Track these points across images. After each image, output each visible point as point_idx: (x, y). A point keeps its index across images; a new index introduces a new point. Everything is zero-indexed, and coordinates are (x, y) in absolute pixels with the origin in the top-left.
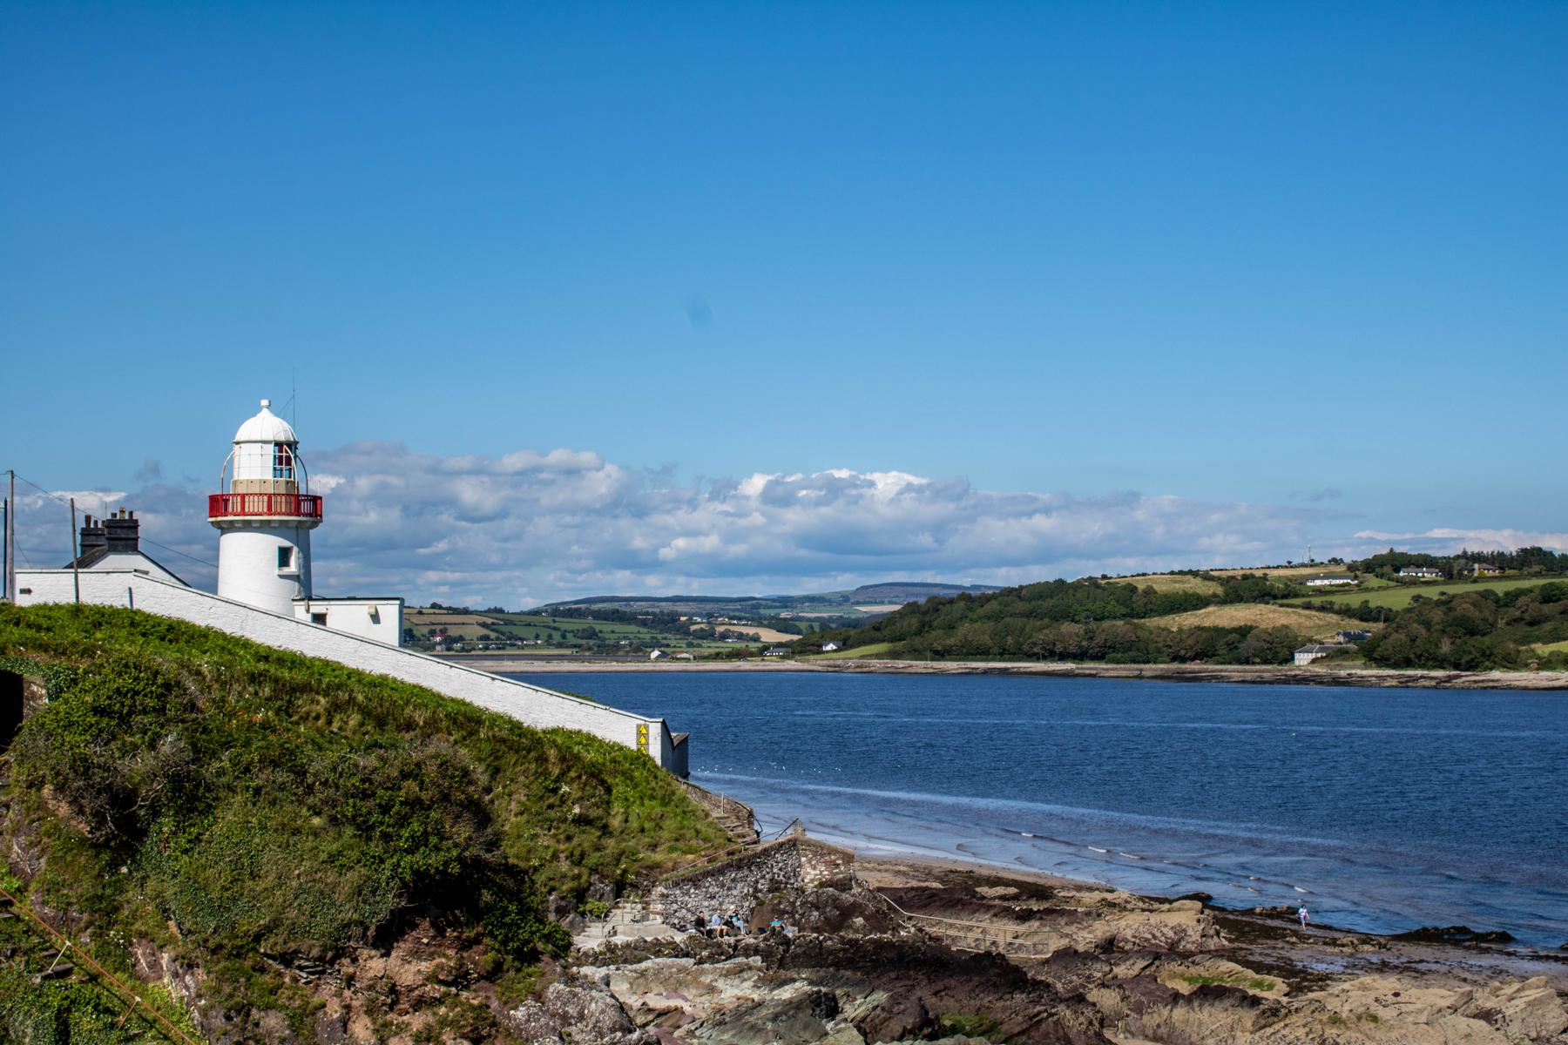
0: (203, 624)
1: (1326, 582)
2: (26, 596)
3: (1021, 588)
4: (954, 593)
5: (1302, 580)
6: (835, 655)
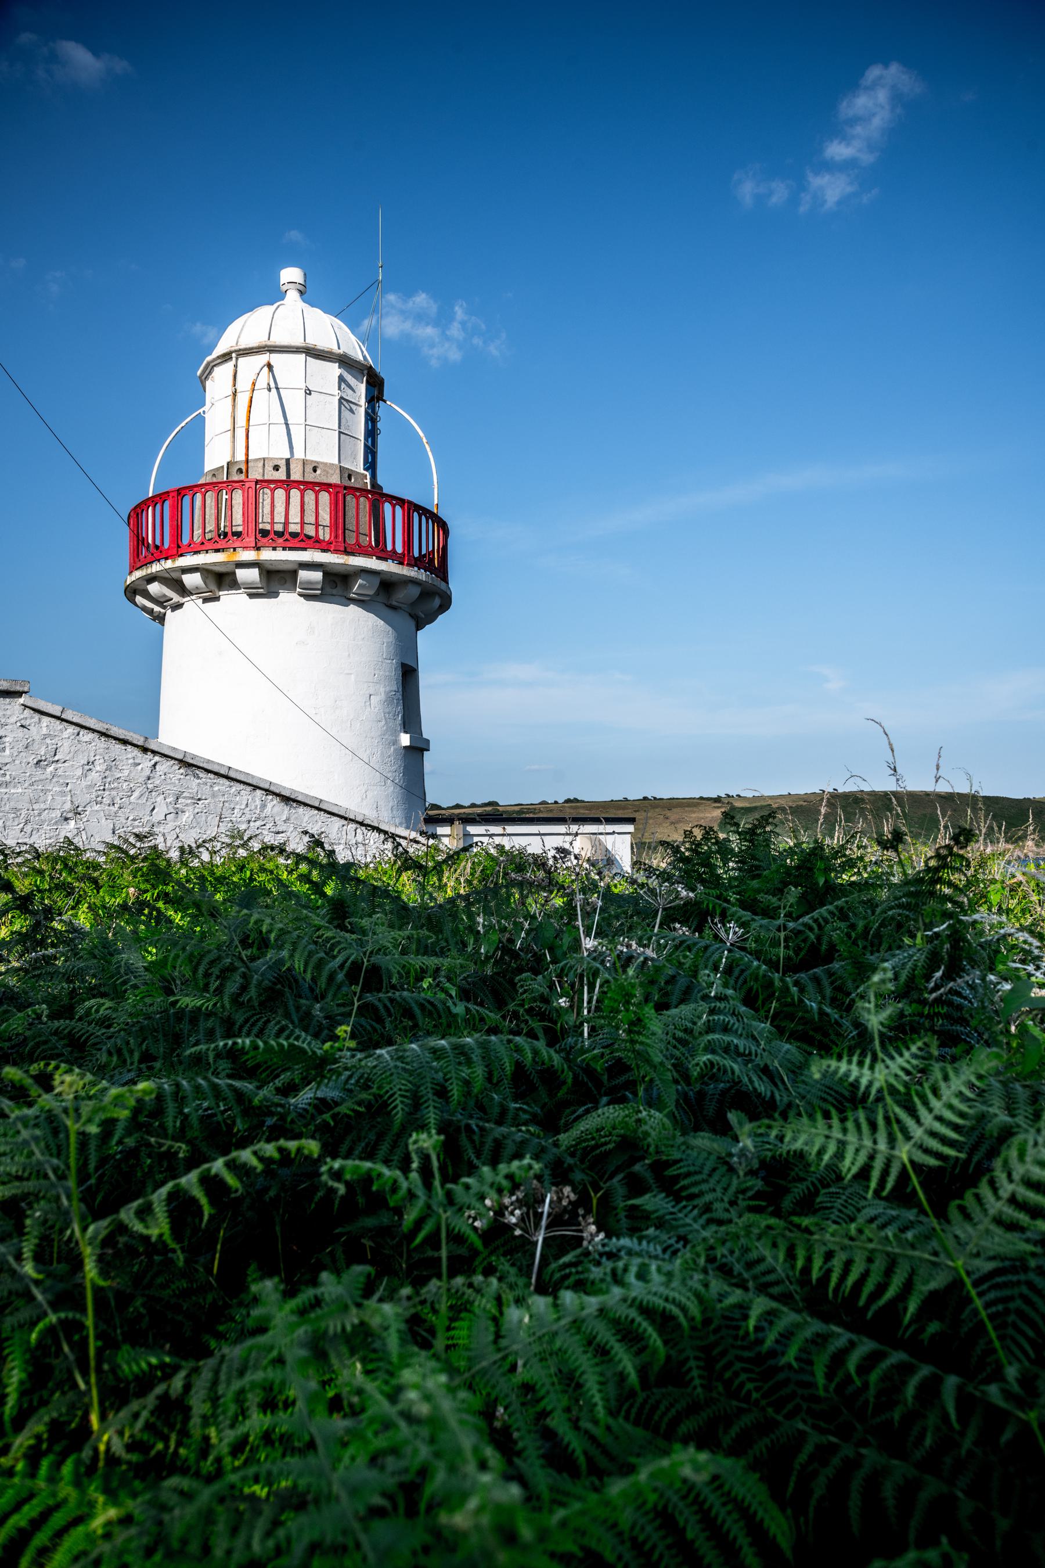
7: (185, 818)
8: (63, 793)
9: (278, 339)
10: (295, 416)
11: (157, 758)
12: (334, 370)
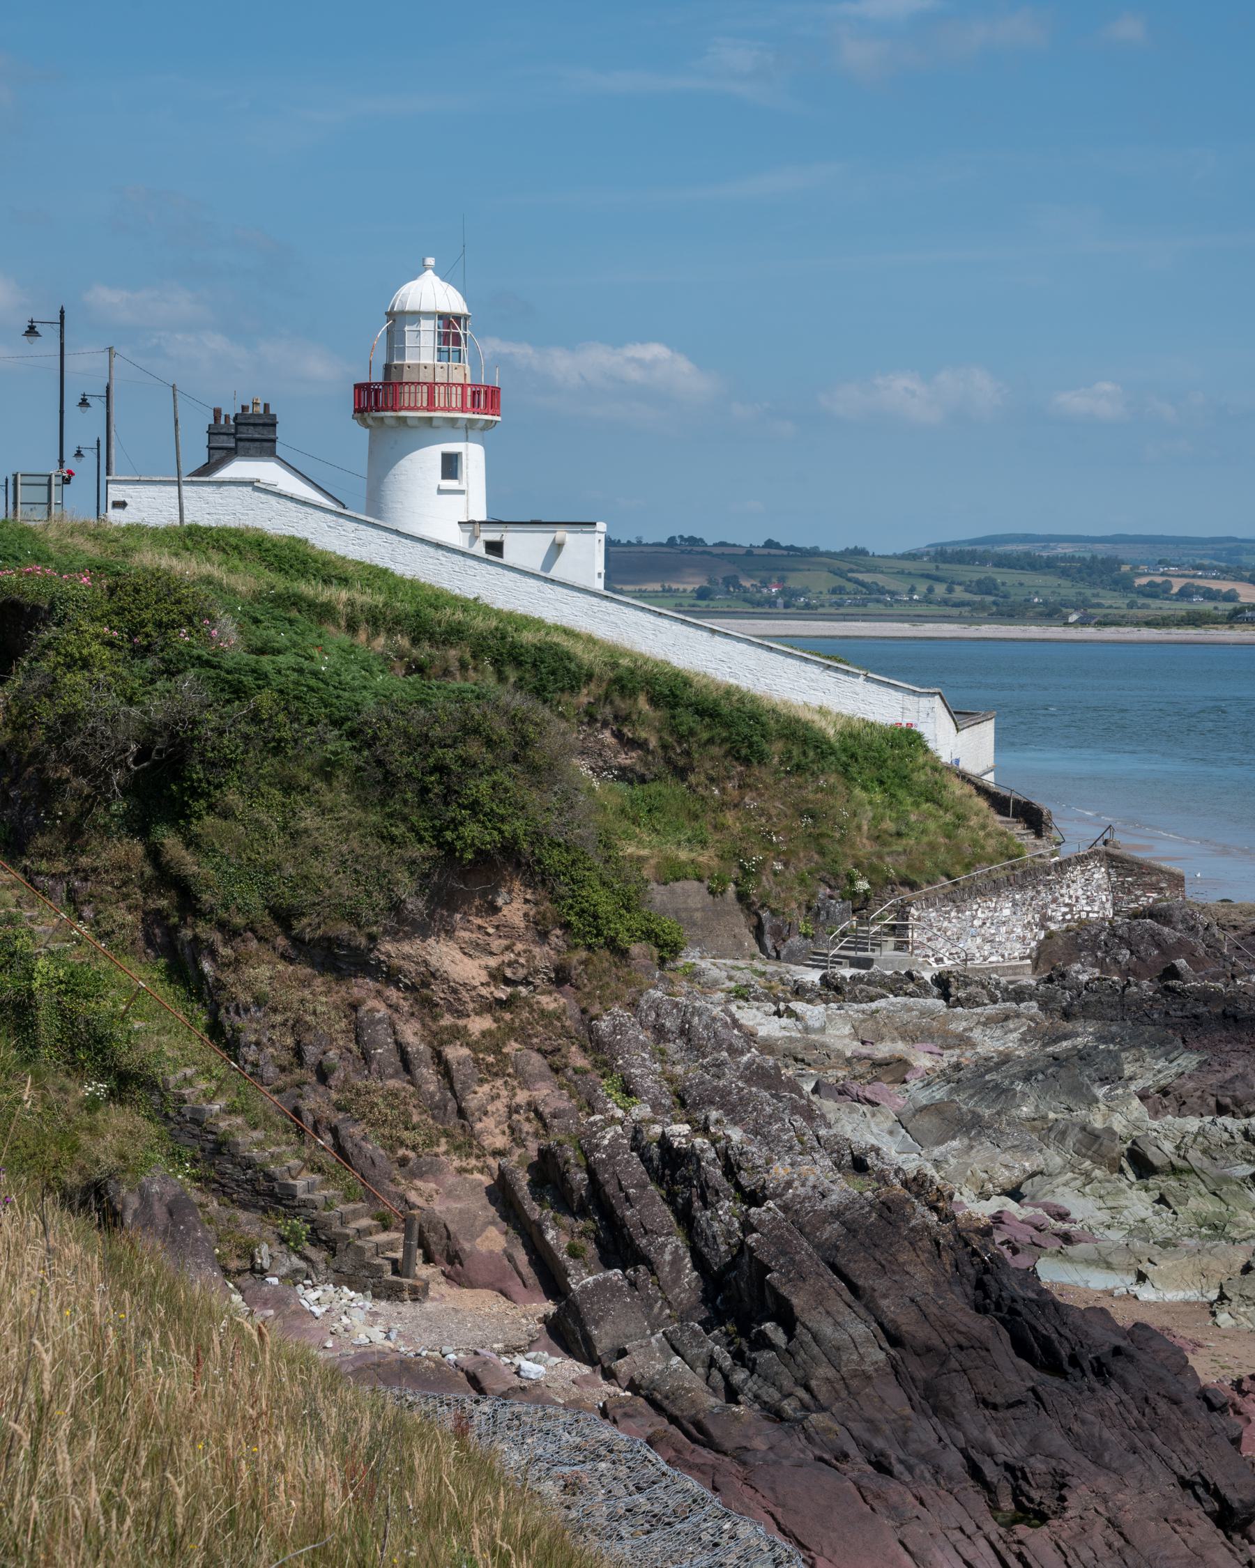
2: (118, 512)
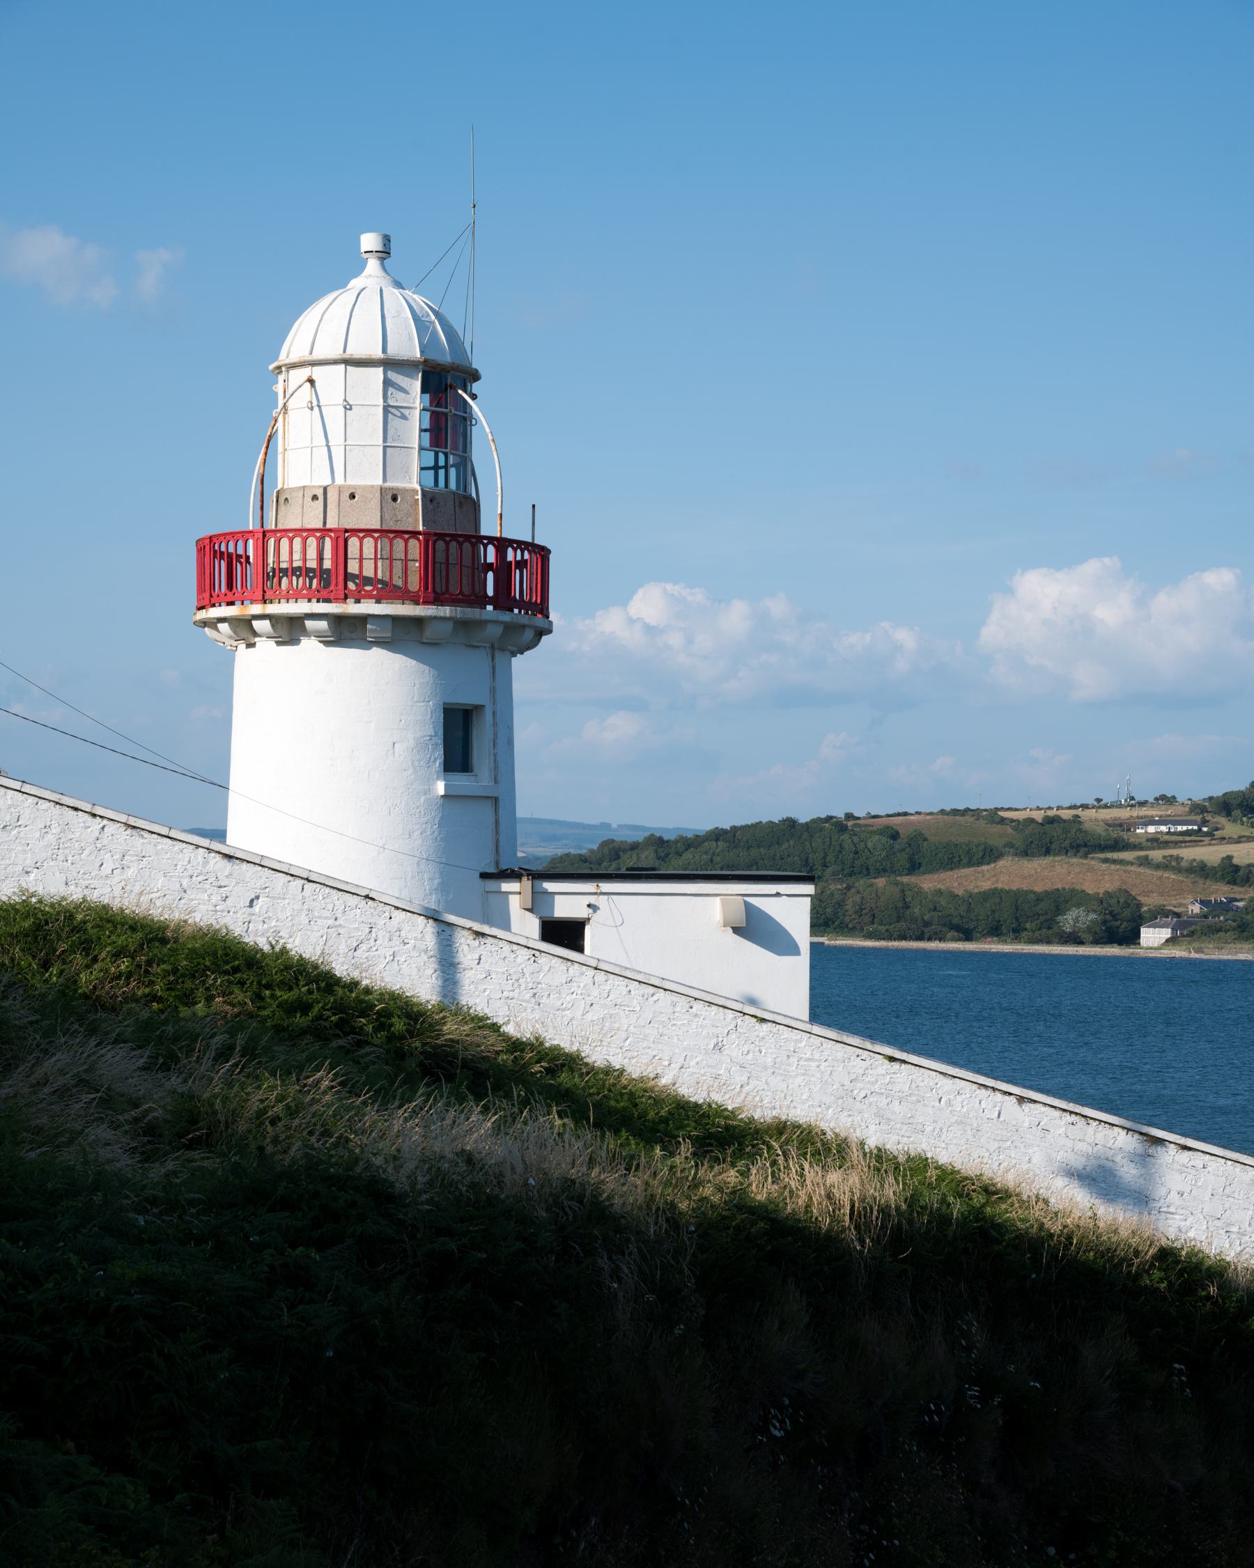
0: (1220, 794)
1: (1164, 828)
3: (734, 829)
4: (640, 837)
5: (1127, 826)
6: (1238, 897)
7: (130, 873)
8: (25, 852)
9: (318, 354)
10: (336, 438)
11: (105, 822)
12: (378, 373)
